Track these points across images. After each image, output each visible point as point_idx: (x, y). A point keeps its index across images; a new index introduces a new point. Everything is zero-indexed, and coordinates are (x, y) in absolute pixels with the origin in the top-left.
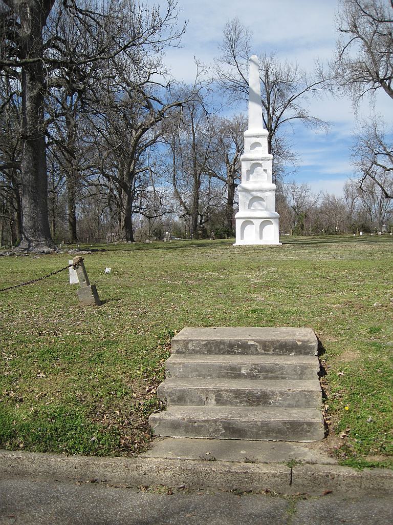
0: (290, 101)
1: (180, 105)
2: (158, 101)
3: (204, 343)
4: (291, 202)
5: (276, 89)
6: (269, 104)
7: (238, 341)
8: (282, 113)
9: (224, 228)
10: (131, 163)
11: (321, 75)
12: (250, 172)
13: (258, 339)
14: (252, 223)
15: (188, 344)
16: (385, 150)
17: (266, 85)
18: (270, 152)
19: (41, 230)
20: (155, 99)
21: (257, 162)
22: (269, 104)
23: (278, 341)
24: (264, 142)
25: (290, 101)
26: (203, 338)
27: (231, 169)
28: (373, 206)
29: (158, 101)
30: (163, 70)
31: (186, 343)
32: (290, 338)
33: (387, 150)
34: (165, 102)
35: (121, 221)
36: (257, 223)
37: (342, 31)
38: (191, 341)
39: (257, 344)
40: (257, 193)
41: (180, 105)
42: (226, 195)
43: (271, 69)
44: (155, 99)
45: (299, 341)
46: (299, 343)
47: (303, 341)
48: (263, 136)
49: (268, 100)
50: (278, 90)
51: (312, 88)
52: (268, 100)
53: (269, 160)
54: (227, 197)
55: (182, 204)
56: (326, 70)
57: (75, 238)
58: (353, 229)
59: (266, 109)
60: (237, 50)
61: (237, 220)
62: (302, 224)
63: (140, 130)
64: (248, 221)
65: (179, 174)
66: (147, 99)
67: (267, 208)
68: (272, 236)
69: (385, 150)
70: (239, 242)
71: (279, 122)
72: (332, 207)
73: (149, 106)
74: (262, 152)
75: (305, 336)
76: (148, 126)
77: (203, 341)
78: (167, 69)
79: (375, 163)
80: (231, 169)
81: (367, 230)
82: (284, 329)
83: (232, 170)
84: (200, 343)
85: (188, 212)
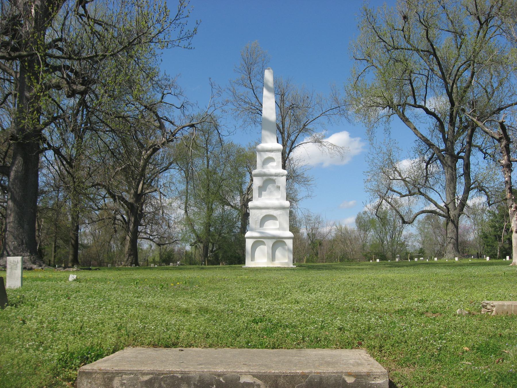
0: (305, 125)
1: (192, 126)
2: (171, 122)
3: (146, 378)
4: (304, 231)
5: (292, 114)
6: (283, 127)
7: (219, 375)
8: (297, 137)
9: (235, 256)
10: (139, 183)
11: (336, 100)
12: (262, 189)
13: (263, 370)
14: (263, 243)
15: (111, 379)
16: (400, 176)
17: (281, 110)
18: (284, 167)
19: (26, 244)
20: (167, 120)
21: (270, 177)
22: (283, 127)
23: (304, 376)
24: (278, 157)
25: (305, 125)
26: (145, 369)
27: (244, 198)
28: (385, 237)
29: (171, 122)
30: (177, 91)
31: (108, 378)
32: (330, 370)
33: (403, 175)
34: (178, 123)
35: (128, 243)
36: (270, 243)
37: (356, 59)
38: (119, 373)
39: (258, 382)
40: (270, 210)
41: (192, 126)
42: (239, 224)
43: (287, 94)
44: (167, 120)
45: (349, 375)
46: (350, 380)
47: (358, 376)
48: (277, 150)
49: (283, 124)
50: (293, 115)
51: (327, 113)
52: (283, 124)
53: (283, 176)
54: (240, 226)
55: (194, 231)
56: (342, 96)
57: (75, 261)
58: (368, 257)
59: (281, 132)
60: (253, 73)
61: (247, 240)
62: (314, 252)
63: (151, 150)
64: (258, 242)
65: (192, 201)
66: (159, 119)
67: (280, 228)
68: (284, 259)
69: (400, 176)
70: (249, 264)
71: (293, 146)
72: (343, 237)
73: (162, 127)
74: (275, 167)
75: (359, 364)
76: (159, 146)
77: (144, 374)
78: (182, 91)
79: (390, 189)
80: (244, 198)
81: (383, 258)
82: (314, 353)
83: (245, 199)
84: (138, 379)
85: (199, 239)
